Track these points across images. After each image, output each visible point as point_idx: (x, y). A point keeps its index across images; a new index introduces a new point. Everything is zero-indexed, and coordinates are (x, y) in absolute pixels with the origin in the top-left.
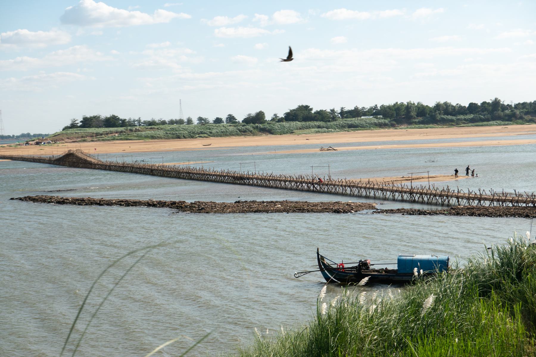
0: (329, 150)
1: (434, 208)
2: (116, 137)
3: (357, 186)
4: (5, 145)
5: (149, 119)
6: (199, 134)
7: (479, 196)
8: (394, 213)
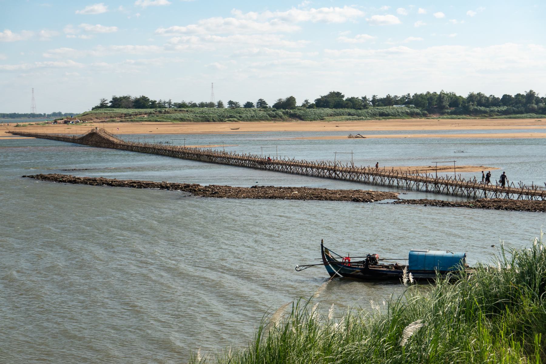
0: (358, 137)
1: (459, 200)
4: (34, 123)
5: (180, 101)
6: (228, 118)
7: (507, 189)
8: (416, 204)
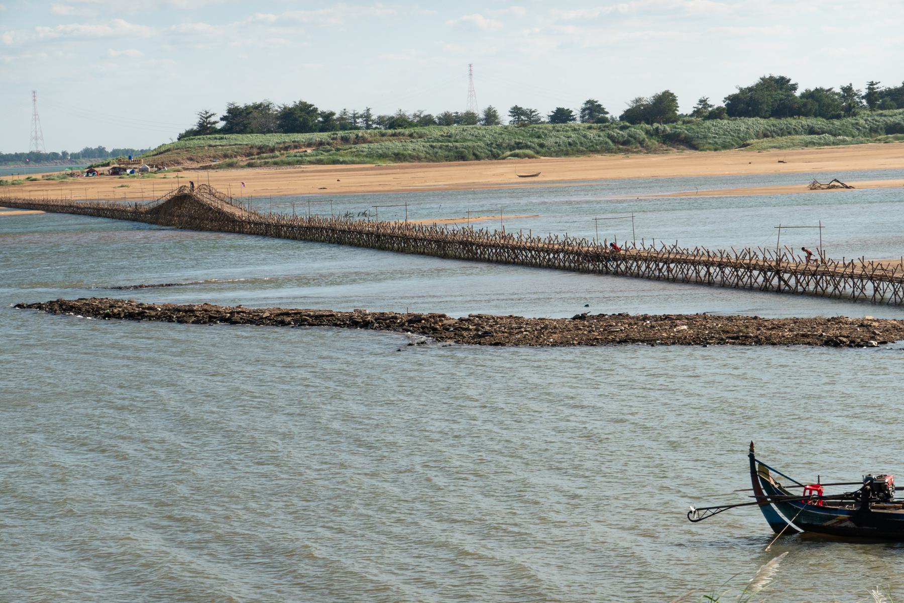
2: (307, 156)
3: (892, 277)
4: (39, 176)
5: (390, 111)
6: (512, 148)
